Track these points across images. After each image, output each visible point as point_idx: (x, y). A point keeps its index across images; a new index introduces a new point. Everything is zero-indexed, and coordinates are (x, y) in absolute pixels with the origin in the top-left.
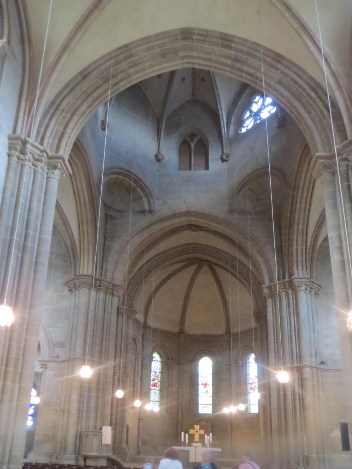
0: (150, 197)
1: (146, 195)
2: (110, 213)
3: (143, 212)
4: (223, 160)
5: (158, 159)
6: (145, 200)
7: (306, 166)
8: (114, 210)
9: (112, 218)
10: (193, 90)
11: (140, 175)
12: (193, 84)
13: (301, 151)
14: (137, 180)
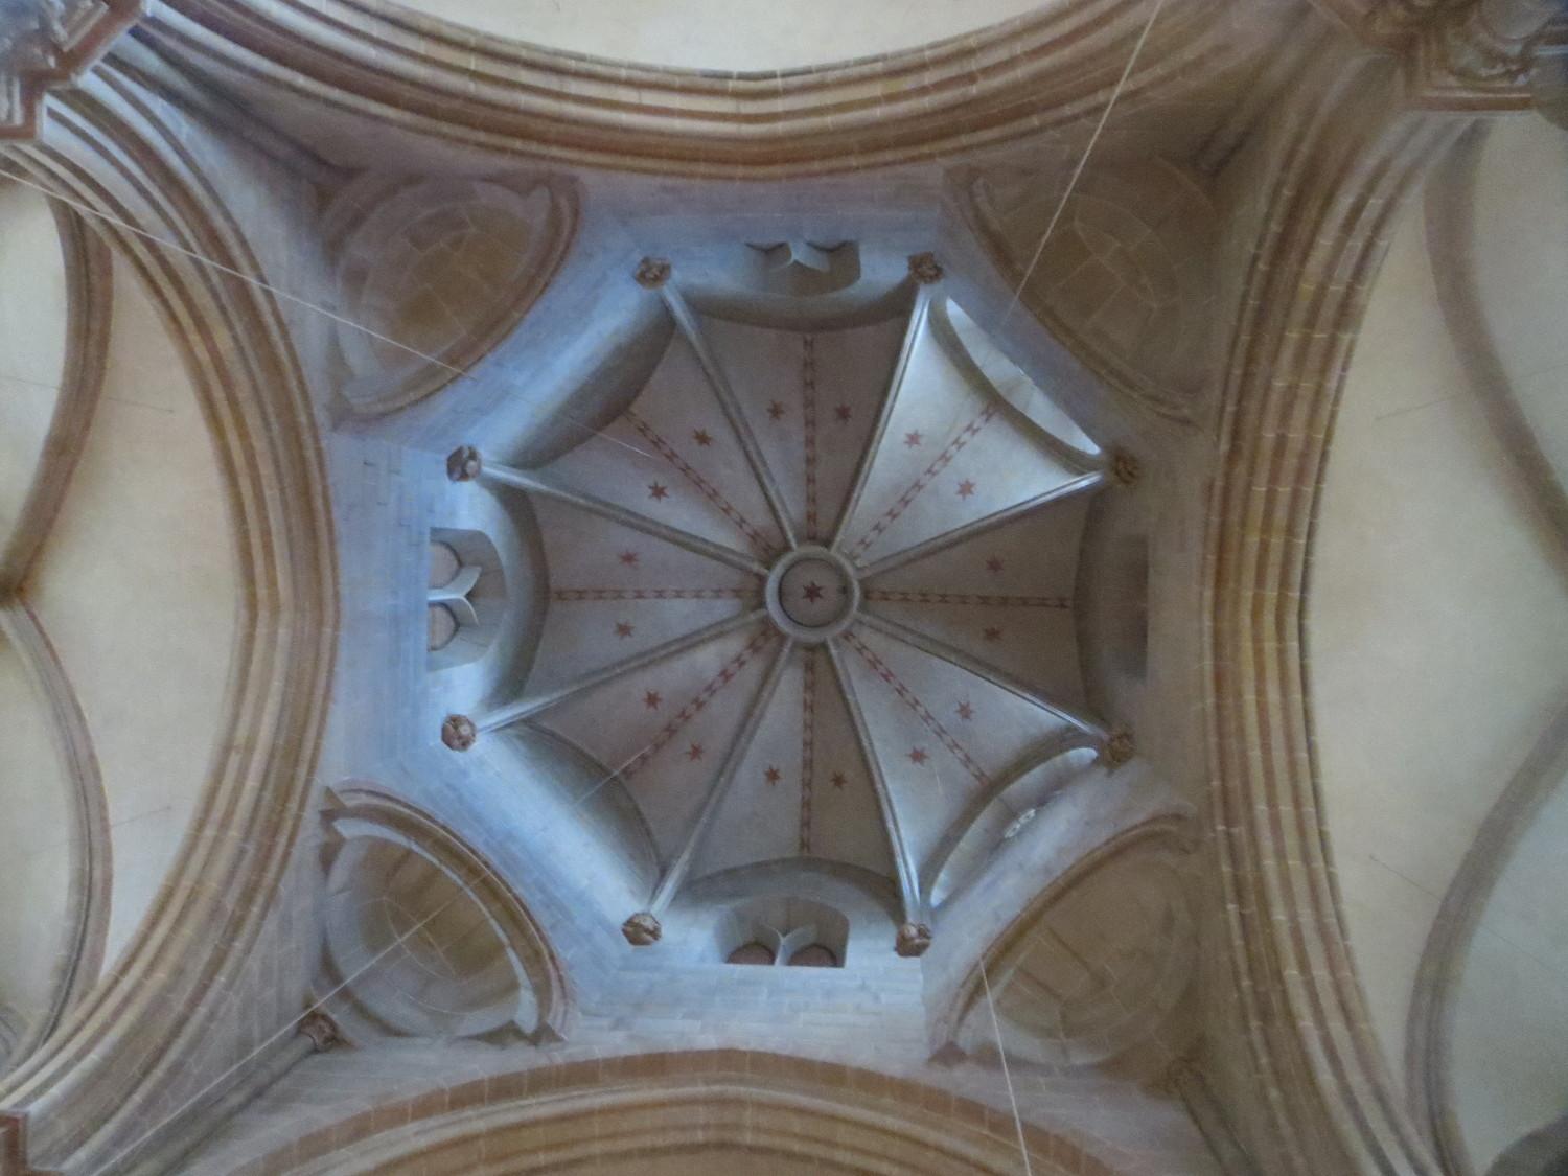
0: (556, 995)
1: (543, 992)
2: (341, 1016)
3: (500, 1036)
4: (908, 948)
5: (638, 933)
6: (526, 998)
7: (1247, 645)
8: (362, 1011)
9: (334, 1041)
10: (806, 824)
11: (544, 918)
12: (806, 804)
13: (1209, 593)
14: (515, 916)
